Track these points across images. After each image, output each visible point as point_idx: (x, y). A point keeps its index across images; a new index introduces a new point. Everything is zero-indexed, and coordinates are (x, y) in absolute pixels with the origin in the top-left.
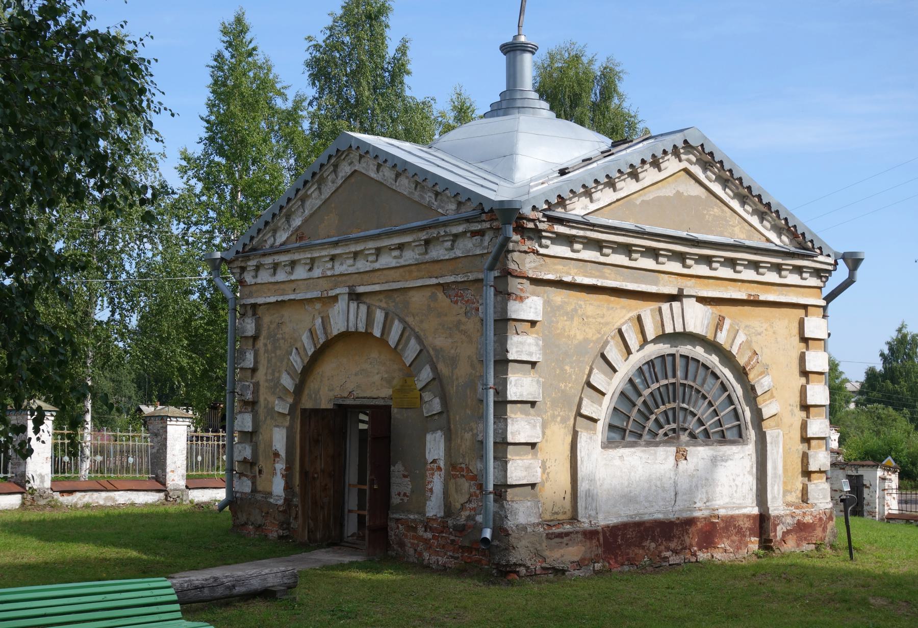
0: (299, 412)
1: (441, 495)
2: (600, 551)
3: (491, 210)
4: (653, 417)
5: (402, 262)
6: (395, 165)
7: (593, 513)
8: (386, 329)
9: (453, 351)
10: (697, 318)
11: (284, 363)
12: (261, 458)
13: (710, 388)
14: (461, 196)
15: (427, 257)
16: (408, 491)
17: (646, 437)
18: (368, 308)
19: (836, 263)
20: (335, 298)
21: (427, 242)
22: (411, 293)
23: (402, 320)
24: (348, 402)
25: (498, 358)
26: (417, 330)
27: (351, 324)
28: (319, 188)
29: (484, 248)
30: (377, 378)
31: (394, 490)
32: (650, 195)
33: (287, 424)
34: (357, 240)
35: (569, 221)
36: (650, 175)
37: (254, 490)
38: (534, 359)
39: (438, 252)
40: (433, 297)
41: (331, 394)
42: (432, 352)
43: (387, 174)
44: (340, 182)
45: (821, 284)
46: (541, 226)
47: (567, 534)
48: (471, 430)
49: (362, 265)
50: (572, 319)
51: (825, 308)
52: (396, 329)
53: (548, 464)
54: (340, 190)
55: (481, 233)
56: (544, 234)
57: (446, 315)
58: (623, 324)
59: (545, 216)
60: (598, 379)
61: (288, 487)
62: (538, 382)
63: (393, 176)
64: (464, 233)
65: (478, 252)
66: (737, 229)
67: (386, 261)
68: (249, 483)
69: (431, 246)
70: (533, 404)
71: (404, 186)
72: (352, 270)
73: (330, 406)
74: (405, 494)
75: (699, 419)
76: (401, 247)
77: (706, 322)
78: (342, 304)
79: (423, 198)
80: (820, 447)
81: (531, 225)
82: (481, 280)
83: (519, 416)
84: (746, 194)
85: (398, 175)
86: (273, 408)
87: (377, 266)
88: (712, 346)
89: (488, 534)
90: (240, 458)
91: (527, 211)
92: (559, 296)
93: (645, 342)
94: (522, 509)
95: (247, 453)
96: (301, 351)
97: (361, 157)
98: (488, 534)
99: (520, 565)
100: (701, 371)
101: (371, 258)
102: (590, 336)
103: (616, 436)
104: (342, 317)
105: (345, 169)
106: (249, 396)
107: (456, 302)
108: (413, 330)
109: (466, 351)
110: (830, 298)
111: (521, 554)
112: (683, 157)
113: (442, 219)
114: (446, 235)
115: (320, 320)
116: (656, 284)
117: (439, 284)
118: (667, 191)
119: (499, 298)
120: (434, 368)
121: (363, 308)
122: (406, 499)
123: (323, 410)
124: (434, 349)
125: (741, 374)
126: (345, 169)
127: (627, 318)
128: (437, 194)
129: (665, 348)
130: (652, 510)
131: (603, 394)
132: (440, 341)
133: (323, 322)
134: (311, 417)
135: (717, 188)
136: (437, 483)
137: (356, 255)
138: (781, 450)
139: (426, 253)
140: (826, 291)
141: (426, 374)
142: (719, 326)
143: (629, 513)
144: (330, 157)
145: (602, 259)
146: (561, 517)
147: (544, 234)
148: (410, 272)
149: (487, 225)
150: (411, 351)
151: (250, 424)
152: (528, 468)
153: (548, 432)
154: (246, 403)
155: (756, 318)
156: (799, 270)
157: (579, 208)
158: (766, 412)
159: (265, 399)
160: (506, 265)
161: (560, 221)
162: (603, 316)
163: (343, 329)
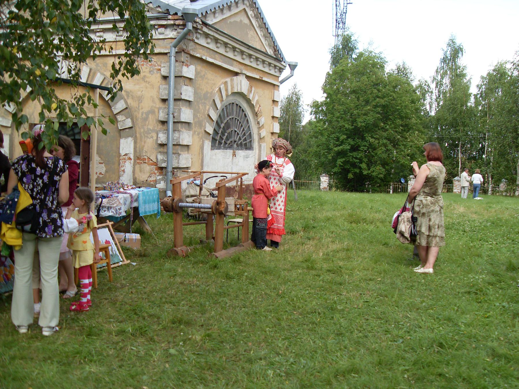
9: (139, 93)
10: (242, 84)
16: (103, 172)
58: (221, 85)
74: (100, 173)
83: (183, 130)
84: (264, 26)
93: (227, 96)
110: (282, 82)
122: (101, 176)
136: (128, 167)
140: (280, 79)
145: (216, 50)
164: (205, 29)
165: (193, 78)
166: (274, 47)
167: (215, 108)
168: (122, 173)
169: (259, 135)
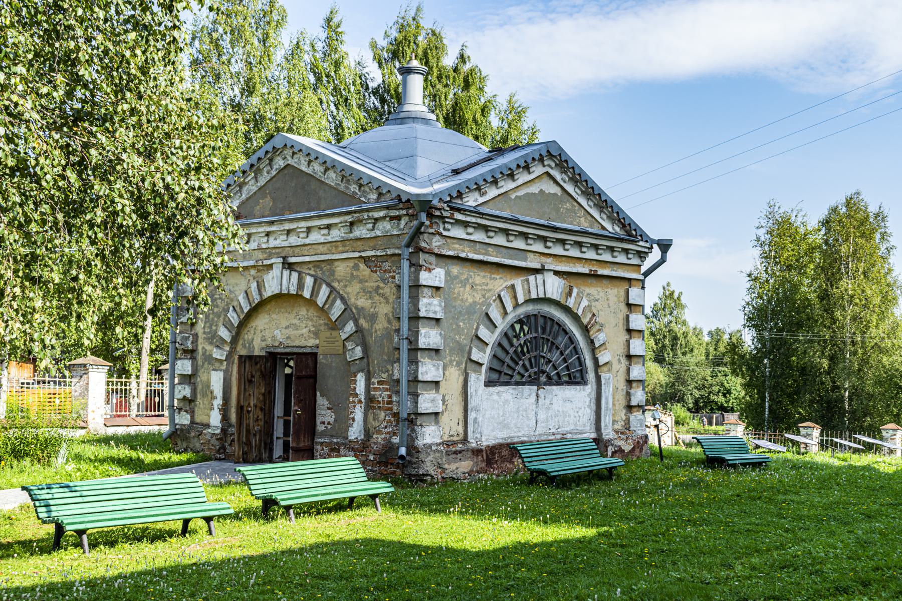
0: (236, 357)
1: (361, 423)
2: (484, 465)
3: (408, 201)
4: (521, 363)
5: (329, 239)
6: (325, 162)
7: (479, 436)
8: (315, 292)
9: (372, 310)
10: (553, 287)
11: (221, 319)
12: (199, 396)
13: (562, 341)
14: (381, 190)
15: (351, 235)
17: (517, 378)
18: (299, 275)
19: (652, 247)
20: (270, 266)
21: (352, 224)
22: (336, 263)
23: (329, 285)
24: (279, 350)
25: (411, 315)
26: (341, 292)
27: (284, 288)
28: (256, 178)
29: (400, 230)
30: (305, 331)
31: (319, 420)
32: (521, 193)
33: (224, 368)
34: (291, 220)
35: (465, 210)
36: (523, 178)
37: (193, 422)
38: (438, 317)
39: (361, 232)
40: (356, 267)
41: (264, 344)
42: (354, 310)
43: (317, 168)
44: (274, 173)
45: (640, 263)
46: (445, 214)
47: (460, 452)
48: (388, 371)
49: (293, 240)
50: (465, 286)
51: (643, 281)
52: (324, 291)
53: (446, 398)
54: (274, 180)
55: (398, 218)
56: (447, 220)
57: (367, 281)
58: (501, 291)
59: (448, 206)
60: (484, 333)
61: (225, 418)
62: (441, 334)
63: (323, 170)
64: (384, 218)
65: (395, 233)
66: (582, 220)
67: (315, 237)
68: (189, 417)
69: (355, 227)
70: (437, 351)
71: (332, 178)
72: (286, 244)
73: (263, 353)
74: (329, 423)
75: (553, 365)
76: (328, 227)
77: (560, 291)
78: (276, 271)
79: (347, 188)
80: (638, 387)
81: (437, 213)
82: (400, 255)
83: (427, 360)
84: (591, 191)
85: (326, 170)
86: (211, 355)
87: (307, 241)
88: (567, 310)
89: (403, 451)
90: (180, 396)
91: (435, 202)
92: (455, 269)
93: (516, 305)
94: (428, 432)
95: (187, 391)
96: (238, 309)
97: (294, 153)
98: (403, 451)
99: (427, 475)
100: (556, 327)
101: (302, 235)
102: (477, 300)
103: (495, 376)
104: (276, 281)
105: (279, 163)
106: (190, 346)
107: (376, 272)
108: (338, 293)
109: (384, 309)
110: (647, 274)
111: (428, 467)
112: (546, 163)
113: (364, 206)
114: (369, 218)
115: (255, 284)
116: (525, 260)
117: (361, 257)
118: (534, 189)
119: (413, 269)
120: (356, 322)
121: (295, 275)
122: (329, 427)
123: (257, 356)
124: (356, 308)
125: (585, 330)
126: (279, 163)
127: (504, 286)
128: (360, 186)
129: (530, 309)
130: (520, 434)
131: (487, 344)
132: (363, 302)
133: (258, 285)
134: (247, 360)
135: (570, 188)
137: (289, 232)
138: (611, 389)
139: (351, 232)
140: (644, 269)
141: (350, 327)
142: (570, 294)
143: (503, 436)
144: (267, 152)
145: (487, 241)
146: (455, 439)
147: (447, 220)
148: (337, 247)
149: (404, 212)
150: (337, 309)
151: (190, 368)
152: (433, 401)
153: (447, 373)
154: (186, 351)
155: (594, 290)
156: (626, 251)
157: (472, 200)
158: (602, 361)
159: (203, 348)
160: (418, 243)
161: (459, 210)
162: (487, 285)
163: (277, 291)
164: (458, 216)
165: (442, 285)
166: (619, 220)
167: (491, 326)
168: (351, 422)
169: (596, 360)
